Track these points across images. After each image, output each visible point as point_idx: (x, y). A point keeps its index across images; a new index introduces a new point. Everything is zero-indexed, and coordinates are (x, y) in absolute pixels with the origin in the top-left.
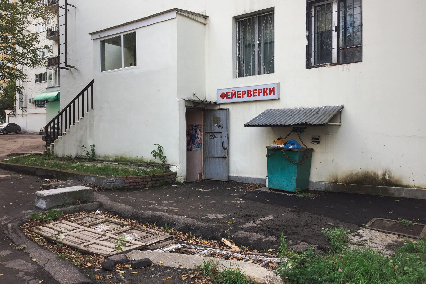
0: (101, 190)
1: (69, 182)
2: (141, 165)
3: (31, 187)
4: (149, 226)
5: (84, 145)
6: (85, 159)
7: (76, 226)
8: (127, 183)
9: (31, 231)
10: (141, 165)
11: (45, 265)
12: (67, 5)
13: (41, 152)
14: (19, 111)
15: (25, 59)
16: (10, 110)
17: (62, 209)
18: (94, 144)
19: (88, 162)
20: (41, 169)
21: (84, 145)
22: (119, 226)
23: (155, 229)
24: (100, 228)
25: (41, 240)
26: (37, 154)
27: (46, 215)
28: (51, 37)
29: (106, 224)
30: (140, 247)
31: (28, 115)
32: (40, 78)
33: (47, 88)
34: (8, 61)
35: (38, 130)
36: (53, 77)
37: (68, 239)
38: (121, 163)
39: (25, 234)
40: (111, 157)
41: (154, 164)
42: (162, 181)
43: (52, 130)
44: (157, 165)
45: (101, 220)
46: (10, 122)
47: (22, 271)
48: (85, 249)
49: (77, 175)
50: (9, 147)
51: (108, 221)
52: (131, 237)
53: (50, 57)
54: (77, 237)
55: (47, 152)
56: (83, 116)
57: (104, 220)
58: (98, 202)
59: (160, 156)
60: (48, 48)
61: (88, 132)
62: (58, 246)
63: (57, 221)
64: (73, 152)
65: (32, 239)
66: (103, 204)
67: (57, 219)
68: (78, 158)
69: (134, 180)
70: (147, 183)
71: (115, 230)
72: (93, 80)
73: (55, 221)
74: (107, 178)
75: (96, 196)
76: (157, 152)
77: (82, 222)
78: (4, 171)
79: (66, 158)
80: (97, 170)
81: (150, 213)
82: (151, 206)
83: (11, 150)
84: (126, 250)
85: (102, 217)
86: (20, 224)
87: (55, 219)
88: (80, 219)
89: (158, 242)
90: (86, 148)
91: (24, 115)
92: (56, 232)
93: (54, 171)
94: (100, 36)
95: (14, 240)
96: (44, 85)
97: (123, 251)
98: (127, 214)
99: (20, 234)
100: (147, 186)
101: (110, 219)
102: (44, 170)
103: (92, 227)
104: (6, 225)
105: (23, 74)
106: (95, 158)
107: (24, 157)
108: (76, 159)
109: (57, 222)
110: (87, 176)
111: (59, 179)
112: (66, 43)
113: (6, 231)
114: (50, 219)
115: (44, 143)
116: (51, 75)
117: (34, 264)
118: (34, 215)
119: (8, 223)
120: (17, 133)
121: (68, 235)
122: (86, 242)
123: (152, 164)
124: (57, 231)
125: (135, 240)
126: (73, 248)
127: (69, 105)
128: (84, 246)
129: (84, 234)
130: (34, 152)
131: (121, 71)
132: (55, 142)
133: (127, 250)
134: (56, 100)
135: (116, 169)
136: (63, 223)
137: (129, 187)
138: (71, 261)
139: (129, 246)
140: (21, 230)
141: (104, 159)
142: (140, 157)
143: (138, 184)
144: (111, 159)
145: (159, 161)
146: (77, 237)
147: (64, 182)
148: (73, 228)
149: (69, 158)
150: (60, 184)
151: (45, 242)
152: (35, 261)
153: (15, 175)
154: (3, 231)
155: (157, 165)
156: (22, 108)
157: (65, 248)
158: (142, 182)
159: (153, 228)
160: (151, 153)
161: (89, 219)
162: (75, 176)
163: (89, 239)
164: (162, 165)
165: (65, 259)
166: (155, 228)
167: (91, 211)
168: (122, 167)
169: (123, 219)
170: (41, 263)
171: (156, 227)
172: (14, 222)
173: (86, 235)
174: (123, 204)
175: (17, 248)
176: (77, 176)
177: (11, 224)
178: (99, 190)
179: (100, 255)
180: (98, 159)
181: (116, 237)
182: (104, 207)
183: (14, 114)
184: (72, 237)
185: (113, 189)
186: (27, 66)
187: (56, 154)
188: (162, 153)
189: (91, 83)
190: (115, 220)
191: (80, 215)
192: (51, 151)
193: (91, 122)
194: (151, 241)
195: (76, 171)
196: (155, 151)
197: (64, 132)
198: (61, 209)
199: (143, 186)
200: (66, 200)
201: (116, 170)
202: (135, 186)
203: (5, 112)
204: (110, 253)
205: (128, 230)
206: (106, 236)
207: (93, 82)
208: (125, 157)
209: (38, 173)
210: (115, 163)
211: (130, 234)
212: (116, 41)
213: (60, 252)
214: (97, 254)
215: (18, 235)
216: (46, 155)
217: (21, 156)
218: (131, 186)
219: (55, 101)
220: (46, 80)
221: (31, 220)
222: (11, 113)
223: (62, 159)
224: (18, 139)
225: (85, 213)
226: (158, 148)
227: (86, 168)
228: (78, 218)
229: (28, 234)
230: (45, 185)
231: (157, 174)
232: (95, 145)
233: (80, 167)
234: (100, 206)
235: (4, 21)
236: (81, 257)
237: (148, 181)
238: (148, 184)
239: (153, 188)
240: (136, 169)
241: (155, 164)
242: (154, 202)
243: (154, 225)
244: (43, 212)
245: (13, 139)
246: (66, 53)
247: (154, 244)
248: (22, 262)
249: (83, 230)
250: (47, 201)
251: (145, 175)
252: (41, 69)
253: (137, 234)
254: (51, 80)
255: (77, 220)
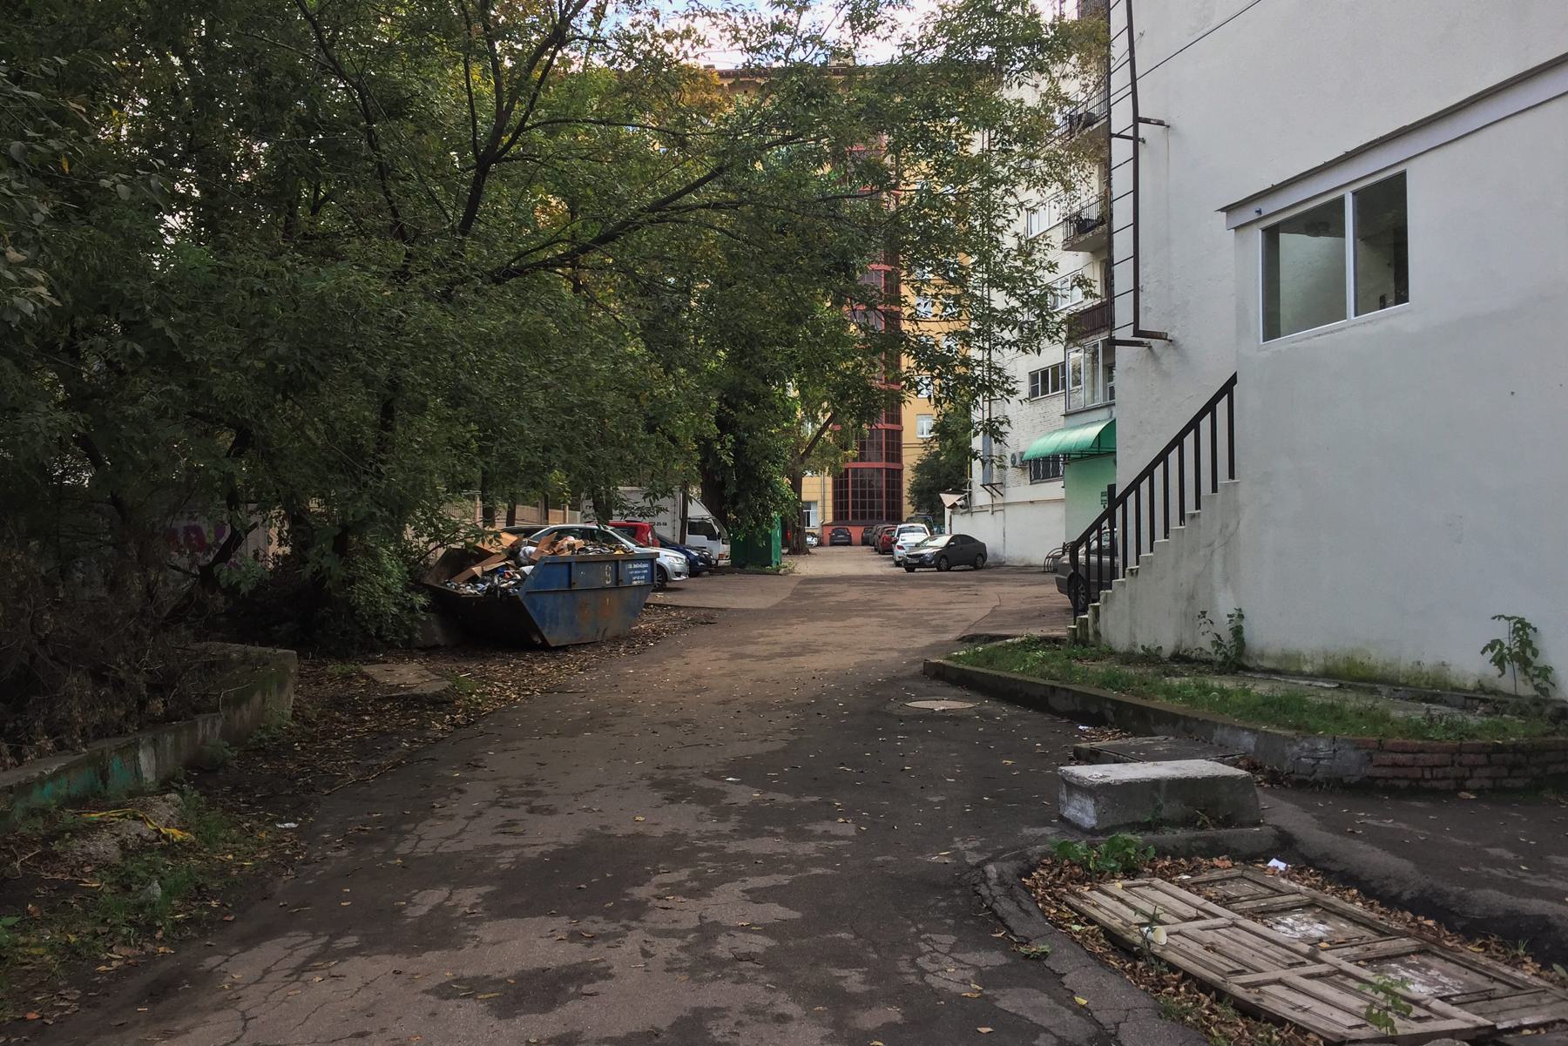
0: (1280, 783)
1: (1160, 742)
2: (1439, 699)
3: (1039, 751)
4: (1497, 951)
5: (1204, 613)
6: (1209, 662)
7: (1205, 907)
8: (1384, 766)
9: (1057, 900)
10: (1439, 699)
11: (1117, 1025)
12: (1141, 125)
13: (1057, 633)
14: (981, 497)
15: (1013, 329)
16: (955, 492)
17: (1149, 835)
18: (1240, 610)
19: (1219, 673)
20: (1064, 689)
21: (1204, 613)
22: (1367, 933)
23: (1525, 967)
24: (1292, 928)
25: (1092, 937)
26: (1046, 640)
27: (1099, 853)
28: (1082, 239)
29: (1314, 917)
30: (1468, 1029)
31: (1008, 509)
32: (1046, 382)
33: (1066, 415)
34: (965, 341)
35: (1039, 556)
36: (1085, 376)
37: (1181, 950)
38: (1350, 687)
39: (1040, 905)
40: (1306, 662)
41: (1497, 698)
42: (1536, 771)
43: (1094, 559)
44: (1510, 699)
45: (1292, 897)
46: (955, 532)
47: (1047, 1030)
48: (1250, 997)
49: (1185, 718)
50: (961, 611)
51: (1320, 907)
52: (1423, 984)
53: (1074, 308)
54: (1211, 948)
55: (1078, 632)
56: (1198, 506)
57: (1306, 899)
58: (1277, 827)
59: (1525, 663)
60: (1085, 282)
61: (1218, 567)
62: (1150, 967)
63: (1135, 877)
64: (1164, 635)
65: (1064, 929)
66: (1295, 837)
67: (1134, 869)
68: (1182, 659)
69: (1411, 755)
70: (1467, 774)
71: (1352, 946)
72: (1236, 373)
73: (1128, 877)
74: (1300, 739)
75: (1263, 804)
76: (1509, 649)
77: (1222, 893)
78: (954, 691)
79: (1142, 655)
80: (1260, 708)
81: (1495, 899)
82: (1499, 872)
83: (966, 624)
84: (1409, 1032)
85: (1293, 885)
86: (1021, 869)
87: (1131, 871)
88: (1212, 882)
89: (1545, 1025)
90: (1212, 622)
91: (995, 509)
92: (1140, 919)
93: (1107, 700)
94: (1259, 212)
95: (1012, 923)
96: (1055, 405)
97: (1400, 1032)
98: (1395, 890)
99: (1027, 905)
100: (1469, 783)
101: (1326, 900)
102: (1075, 693)
103: (1262, 919)
104: (980, 866)
105: (1007, 378)
106: (1246, 663)
107: (1007, 647)
108: (1178, 662)
109: (1138, 881)
110: (1223, 725)
111: (1126, 728)
112: (1136, 256)
113: (983, 886)
114: (1113, 865)
115: (1064, 601)
116: (1077, 370)
117: (1083, 1016)
118: (1062, 847)
119: (986, 862)
120: (976, 568)
121: (1178, 933)
122: (1249, 970)
123: (1482, 697)
124: (1144, 914)
125: (1442, 999)
126: (1205, 986)
127: (1148, 472)
128: (1244, 985)
129: (1234, 940)
130: (1037, 632)
131: (1344, 329)
132: (1102, 597)
133: (1415, 1032)
134: (1102, 451)
135: (1332, 707)
136: (1157, 889)
137: (1390, 781)
138: (1206, 1033)
139: (1419, 1019)
140: (1028, 890)
141: (1280, 668)
142: (1429, 662)
143: (1427, 775)
144: (1307, 669)
145: (1520, 684)
146: (1211, 948)
147: (1145, 741)
148: (1193, 912)
149: (1150, 658)
150: (1134, 748)
151: (1104, 945)
152: (1083, 1006)
153: (988, 705)
154: (975, 885)
155: (1510, 699)
156: (991, 485)
157: (1174, 980)
158: (1448, 769)
159: (1516, 963)
160: (1483, 653)
161: (1248, 888)
162: (1181, 723)
163: (1259, 962)
164: (1537, 704)
165: (1183, 1019)
166: (1525, 962)
167: (1252, 857)
168: (1354, 701)
169: (1381, 905)
170: (1103, 1017)
171: (1528, 960)
172: (1004, 860)
173: (1246, 946)
174: (1377, 850)
175: (1022, 949)
176: (1188, 725)
177: (996, 868)
178: (1272, 784)
179: (1306, 1031)
180: (1258, 666)
181: (1366, 973)
182: (1301, 850)
183: (967, 507)
184: (1194, 945)
185: (1328, 785)
186: (1020, 352)
187: (1108, 641)
188: (1535, 653)
189: (1228, 388)
190: (1350, 906)
191: (1212, 867)
192: (1091, 631)
193: (1227, 527)
194: (1513, 1013)
195: (1185, 706)
196: (1502, 645)
197: (1132, 565)
198: (1146, 837)
199: (1452, 785)
200: (1159, 808)
201: (1333, 713)
202: (1417, 780)
203: (940, 500)
204: (1348, 1031)
205: (1407, 954)
206: (1321, 962)
207: (1233, 380)
208: (1365, 661)
209: (1057, 702)
210: (1326, 685)
211: (1419, 970)
212: (1322, 221)
213: (1159, 989)
214: (1296, 1025)
215: (1019, 905)
216: (1076, 642)
217: (1000, 643)
218: (1398, 778)
219: (1091, 456)
220: (1064, 387)
221: (1055, 862)
222: (959, 503)
223: (1129, 658)
224: (982, 588)
225: (1228, 863)
226: (1516, 630)
227: (1215, 696)
228: (1205, 877)
229: (1047, 908)
230: (1083, 745)
231: (1513, 739)
232: (1245, 612)
233: (1193, 691)
234: (1285, 845)
235: (950, 213)
236: (1237, 1025)
237: (1473, 767)
238: (1471, 777)
239: (1496, 793)
240: (1418, 713)
241: (1503, 699)
242: (1510, 855)
243: (1517, 949)
244: (1089, 838)
245: (968, 586)
246: (1136, 290)
247: (1527, 1032)
248: (1044, 1000)
249: (1230, 926)
250: (1097, 801)
251: (1461, 739)
252: (1052, 353)
253: (1447, 975)
254: (1079, 387)
255: (1204, 882)
